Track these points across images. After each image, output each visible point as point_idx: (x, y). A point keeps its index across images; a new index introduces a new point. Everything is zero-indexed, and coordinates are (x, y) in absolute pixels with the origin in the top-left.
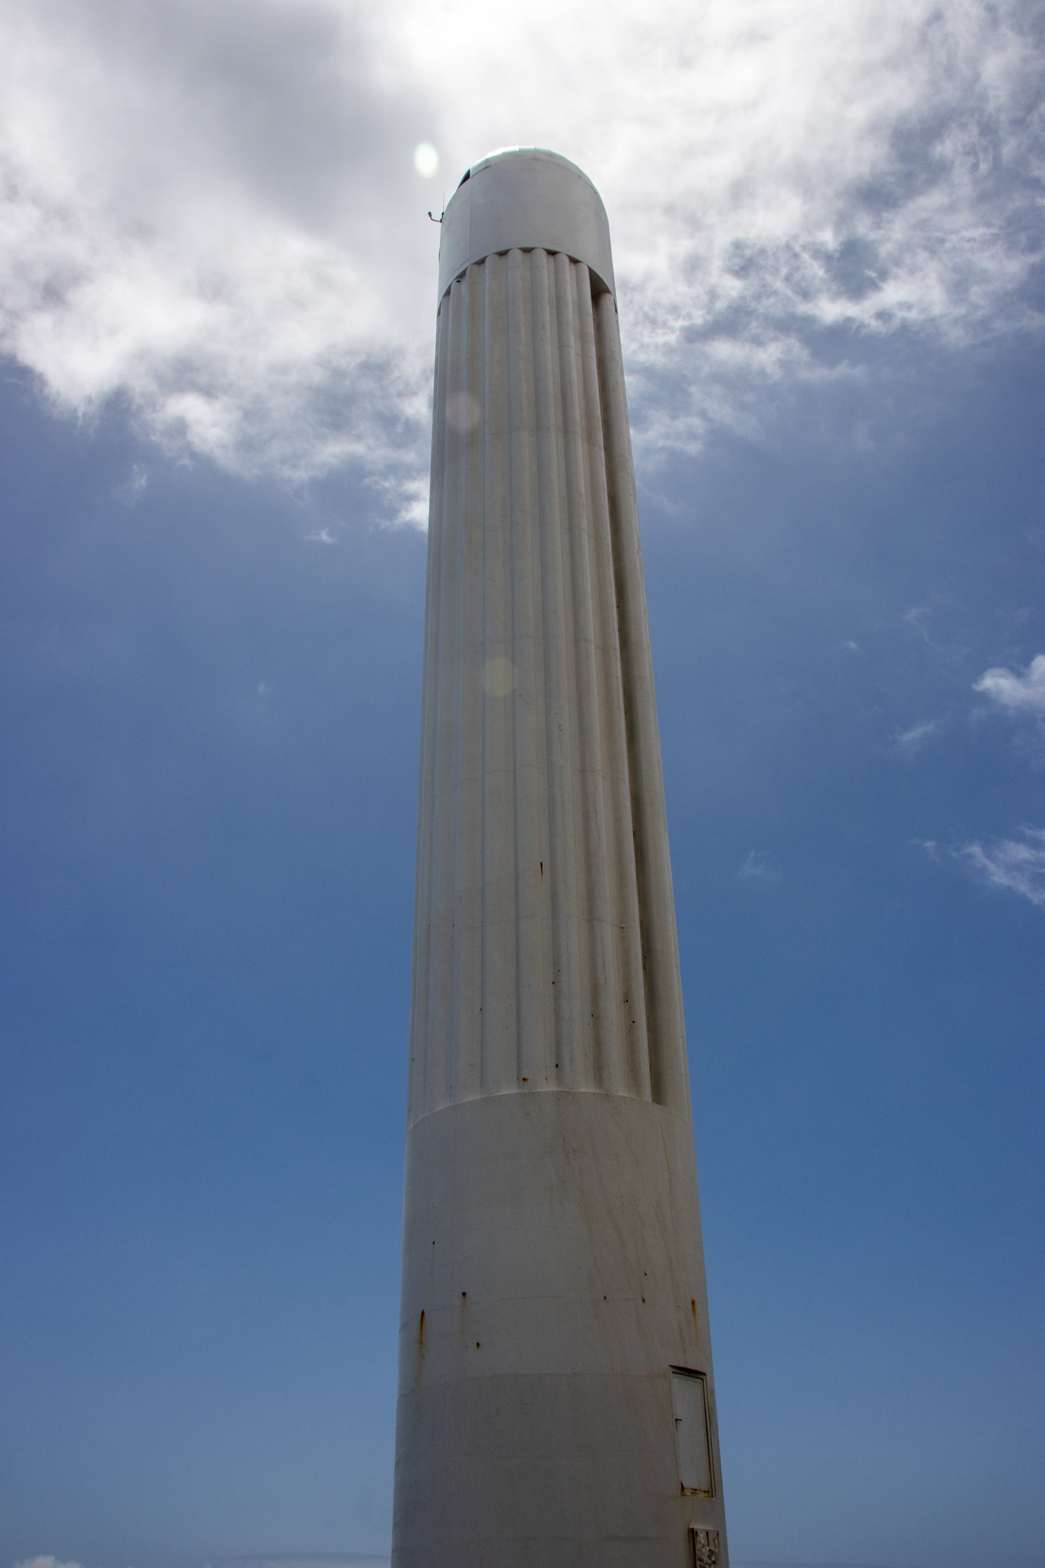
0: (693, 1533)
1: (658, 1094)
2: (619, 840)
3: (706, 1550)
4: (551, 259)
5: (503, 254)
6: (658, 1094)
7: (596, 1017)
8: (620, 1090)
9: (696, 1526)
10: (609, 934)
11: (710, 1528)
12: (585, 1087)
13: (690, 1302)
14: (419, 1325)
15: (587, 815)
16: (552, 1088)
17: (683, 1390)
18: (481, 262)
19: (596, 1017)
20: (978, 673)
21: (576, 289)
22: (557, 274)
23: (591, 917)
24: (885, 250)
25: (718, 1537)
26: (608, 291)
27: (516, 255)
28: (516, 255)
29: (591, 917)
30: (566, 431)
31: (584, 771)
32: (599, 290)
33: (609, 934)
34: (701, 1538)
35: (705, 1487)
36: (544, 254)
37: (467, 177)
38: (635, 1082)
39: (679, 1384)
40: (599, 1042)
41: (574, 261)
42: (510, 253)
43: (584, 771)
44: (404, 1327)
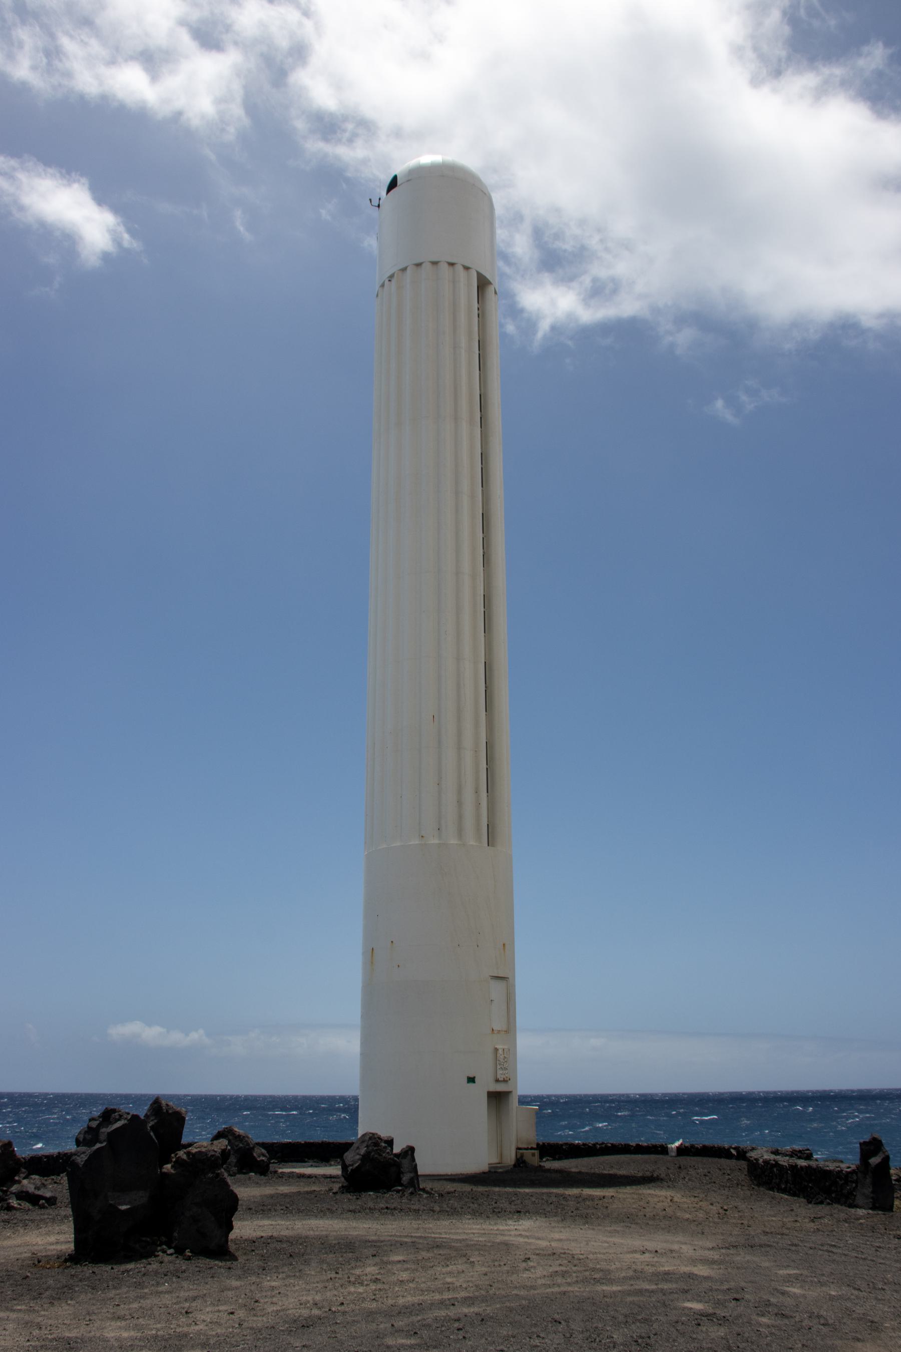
0: (496, 1050)
1: (491, 841)
3: (502, 1057)
5: (419, 265)
6: (491, 841)
7: (460, 803)
10: (468, 756)
11: (506, 1047)
12: (453, 841)
14: (371, 955)
15: (459, 686)
16: (436, 841)
17: (497, 989)
18: (404, 270)
19: (460, 803)
23: (459, 747)
24: (244, 1228)
25: (511, 1051)
27: (427, 267)
28: (427, 267)
29: (459, 747)
31: (459, 659)
32: (483, 284)
33: (468, 756)
34: (500, 1051)
35: (505, 1028)
36: (446, 265)
39: (494, 984)
40: (460, 817)
42: (424, 265)
44: (364, 953)
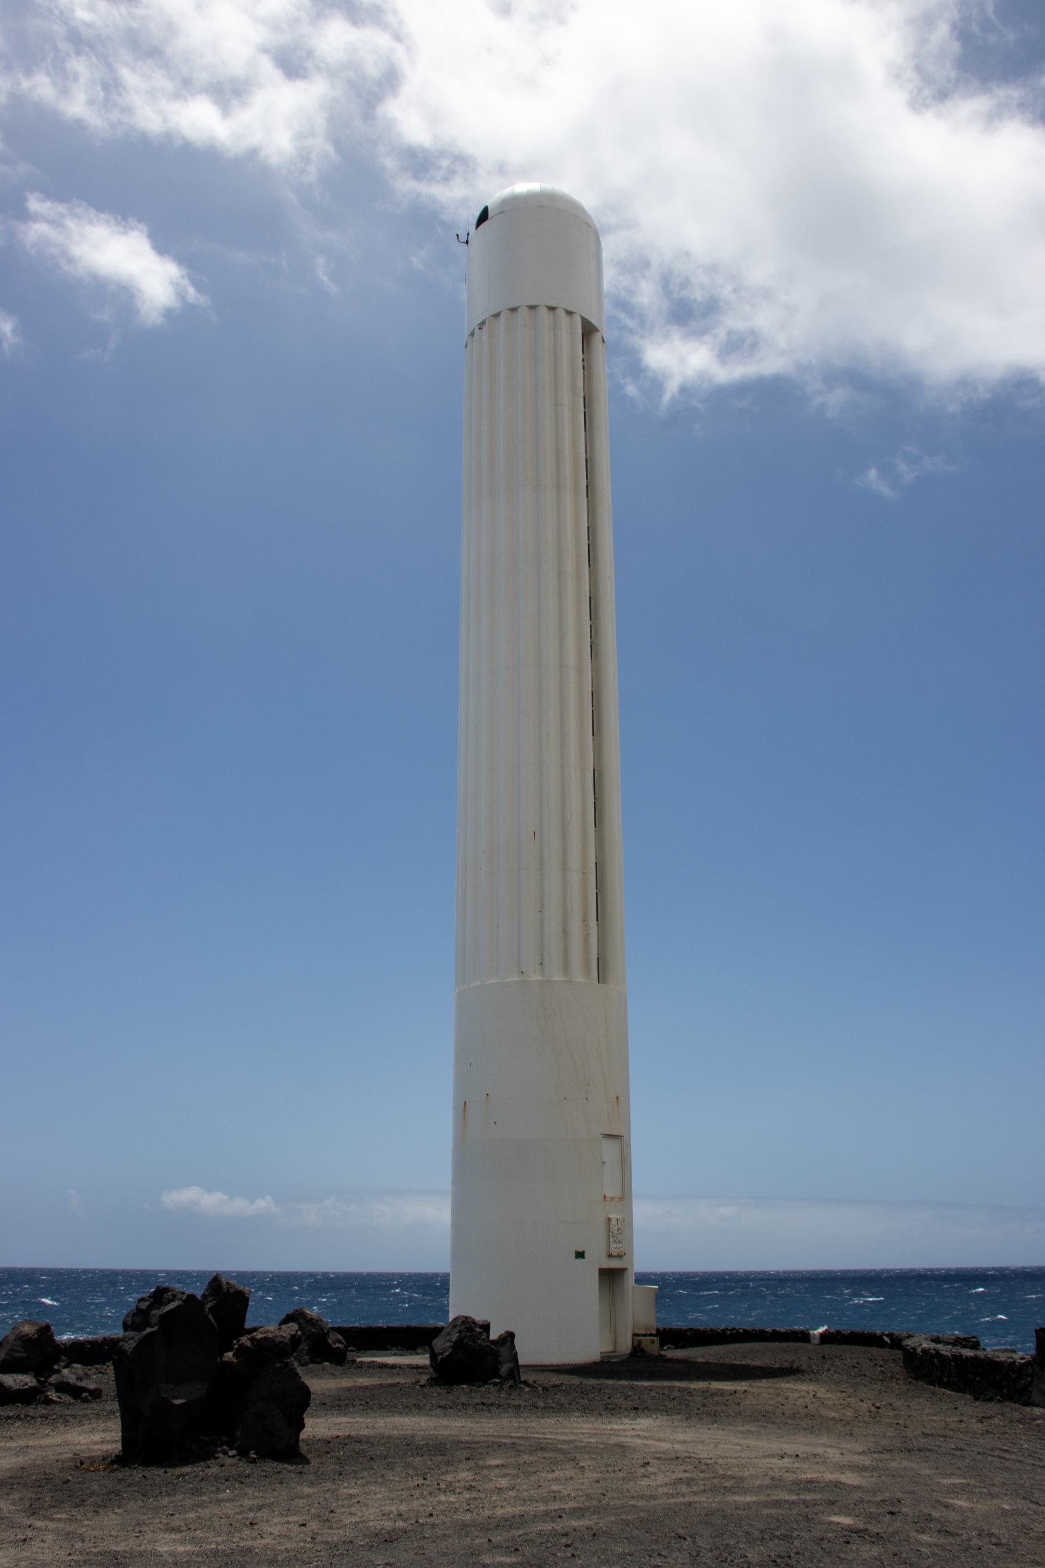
0: (609, 1220)
2: (584, 815)
3: (616, 1228)
4: (551, 313)
5: (514, 310)
6: (602, 976)
7: (565, 933)
8: (579, 979)
9: (610, 1216)
10: (575, 879)
11: (620, 1216)
12: (558, 977)
13: (615, 1097)
14: (463, 1111)
17: (610, 1150)
18: (497, 315)
19: (565, 933)
20: (221, 1355)
21: (570, 335)
22: (555, 328)
23: (565, 868)
26: (597, 330)
27: (523, 312)
28: (523, 312)
30: (559, 487)
31: (563, 766)
32: (588, 331)
33: (575, 879)
34: (614, 1222)
36: (546, 310)
37: (484, 216)
38: (587, 973)
40: (566, 949)
41: (569, 313)
43: (563, 766)
